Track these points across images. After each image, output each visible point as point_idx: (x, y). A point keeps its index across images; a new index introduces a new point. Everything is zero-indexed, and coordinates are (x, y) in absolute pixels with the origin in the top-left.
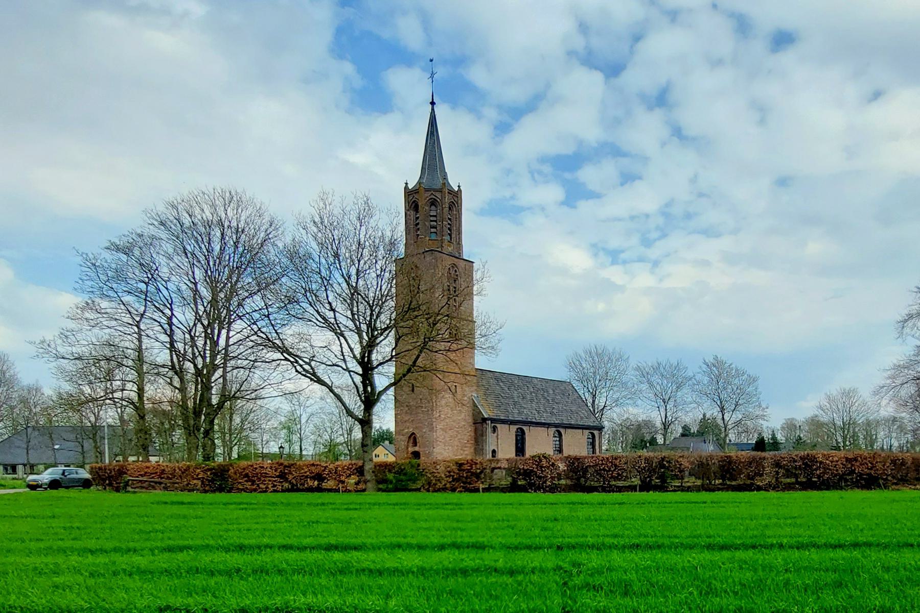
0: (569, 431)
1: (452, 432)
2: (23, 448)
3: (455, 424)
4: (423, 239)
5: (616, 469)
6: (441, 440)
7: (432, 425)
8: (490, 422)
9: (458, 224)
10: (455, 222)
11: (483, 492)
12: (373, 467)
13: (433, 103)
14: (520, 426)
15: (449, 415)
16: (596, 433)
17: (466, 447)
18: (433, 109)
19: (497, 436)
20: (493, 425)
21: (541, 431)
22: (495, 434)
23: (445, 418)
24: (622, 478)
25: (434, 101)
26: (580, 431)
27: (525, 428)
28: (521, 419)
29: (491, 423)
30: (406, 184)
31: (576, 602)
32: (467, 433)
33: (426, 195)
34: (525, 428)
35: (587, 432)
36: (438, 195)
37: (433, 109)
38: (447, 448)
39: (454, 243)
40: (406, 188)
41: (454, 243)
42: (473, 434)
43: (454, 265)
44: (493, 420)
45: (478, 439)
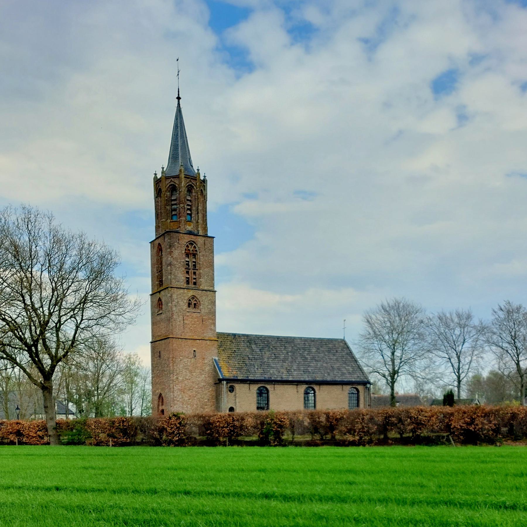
0: (325, 388)
1: (192, 392)
2: (355, 394)
3: (194, 385)
4: (164, 223)
5: (228, 425)
6: (178, 399)
7: (170, 386)
8: (225, 382)
9: (196, 204)
10: (194, 202)
11: (18, 444)
12: (379, 419)
13: (179, 98)
14: (263, 385)
15: (187, 377)
16: (360, 388)
17: (206, 405)
18: (179, 104)
19: (235, 395)
20: (229, 385)
21: (290, 390)
22: (233, 393)
23: (183, 380)
24: (234, 434)
25: (180, 96)
26: (340, 387)
27: (268, 387)
28: (263, 378)
29: (227, 383)
30: (156, 174)
31: (13, 515)
32: (208, 393)
33: (167, 182)
34: (268, 387)
35: (347, 388)
36: (177, 181)
37: (179, 104)
38: (185, 406)
39: (194, 221)
40: (155, 177)
41: (194, 221)
42: (214, 394)
43: (191, 243)
44: (228, 381)
45: (217, 398)
